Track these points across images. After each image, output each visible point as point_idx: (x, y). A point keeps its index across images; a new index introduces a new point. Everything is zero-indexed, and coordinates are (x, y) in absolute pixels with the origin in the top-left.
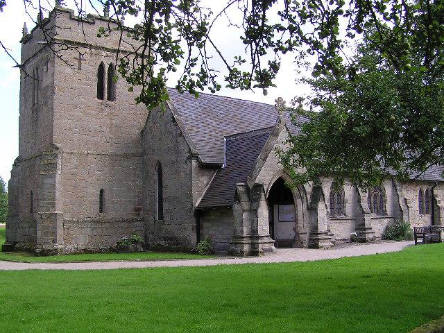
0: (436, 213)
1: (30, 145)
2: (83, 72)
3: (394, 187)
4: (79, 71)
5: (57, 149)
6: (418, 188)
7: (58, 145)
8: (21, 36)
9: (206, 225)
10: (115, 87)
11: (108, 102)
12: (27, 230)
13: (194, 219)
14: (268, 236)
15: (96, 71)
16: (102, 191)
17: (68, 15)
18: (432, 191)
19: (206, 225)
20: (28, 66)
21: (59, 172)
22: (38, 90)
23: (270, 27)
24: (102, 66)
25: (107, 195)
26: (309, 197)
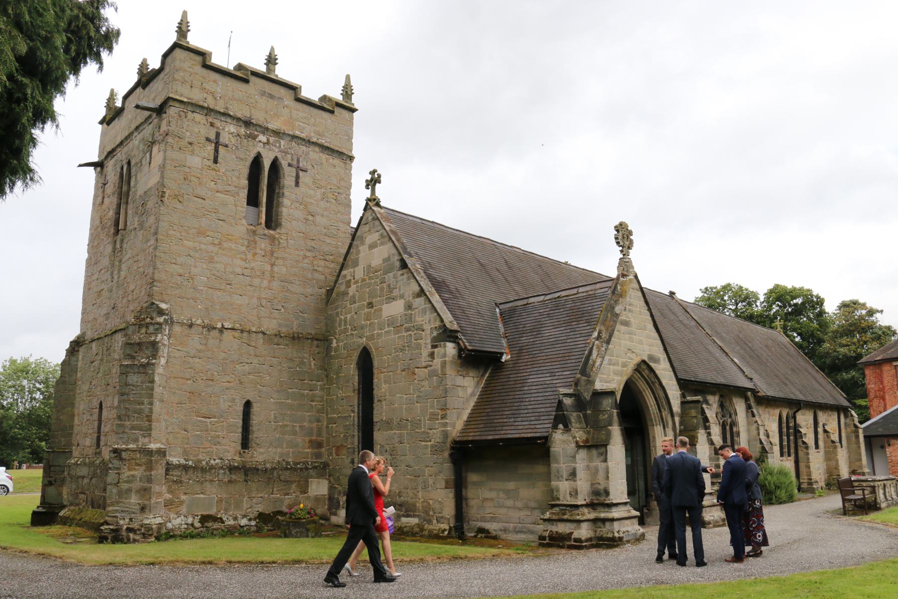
0: (801, 454)
1: (104, 311)
2: (222, 167)
3: (749, 407)
4: (214, 166)
5: (161, 312)
6: (777, 411)
7: (163, 306)
8: (102, 112)
9: (473, 477)
10: (279, 205)
11: (267, 231)
12: (86, 481)
13: (448, 466)
14: (625, 504)
15: (246, 172)
16: (248, 405)
17: (199, 59)
18: (794, 417)
19: (473, 477)
20: (110, 165)
21: (163, 361)
22: (127, 203)
23: (382, 244)
24: (257, 162)
25: (255, 409)
26: (677, 419)
